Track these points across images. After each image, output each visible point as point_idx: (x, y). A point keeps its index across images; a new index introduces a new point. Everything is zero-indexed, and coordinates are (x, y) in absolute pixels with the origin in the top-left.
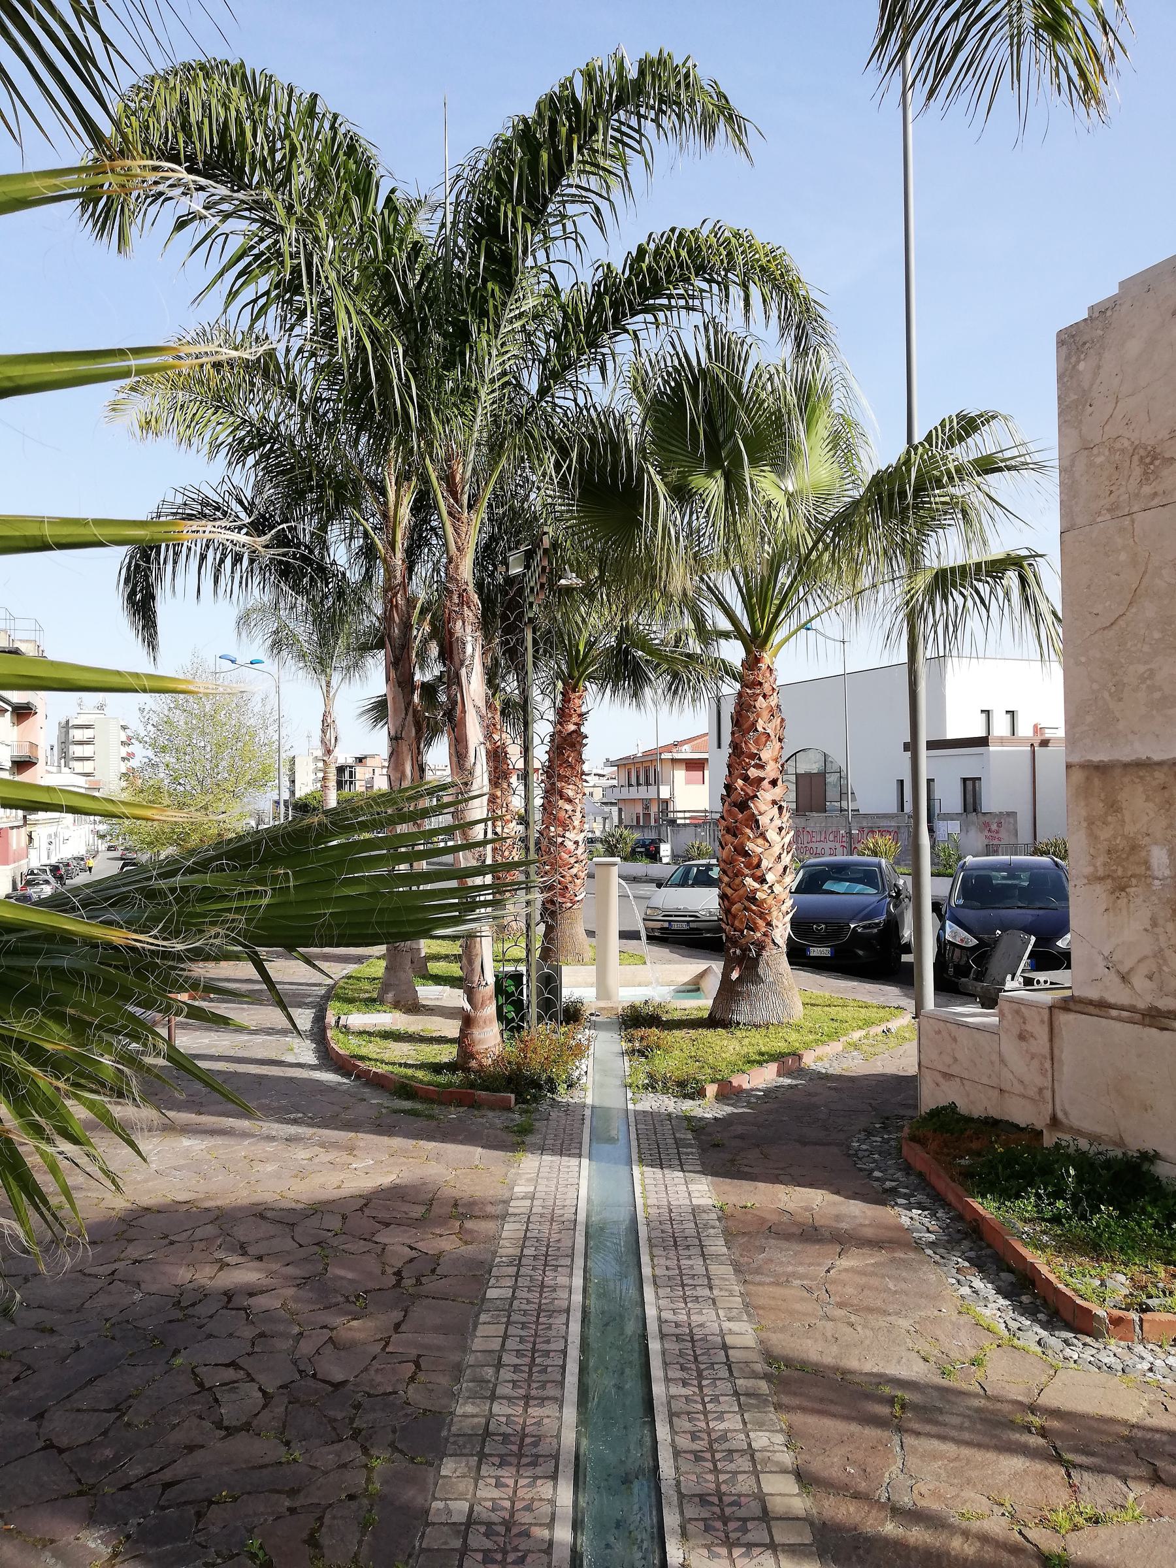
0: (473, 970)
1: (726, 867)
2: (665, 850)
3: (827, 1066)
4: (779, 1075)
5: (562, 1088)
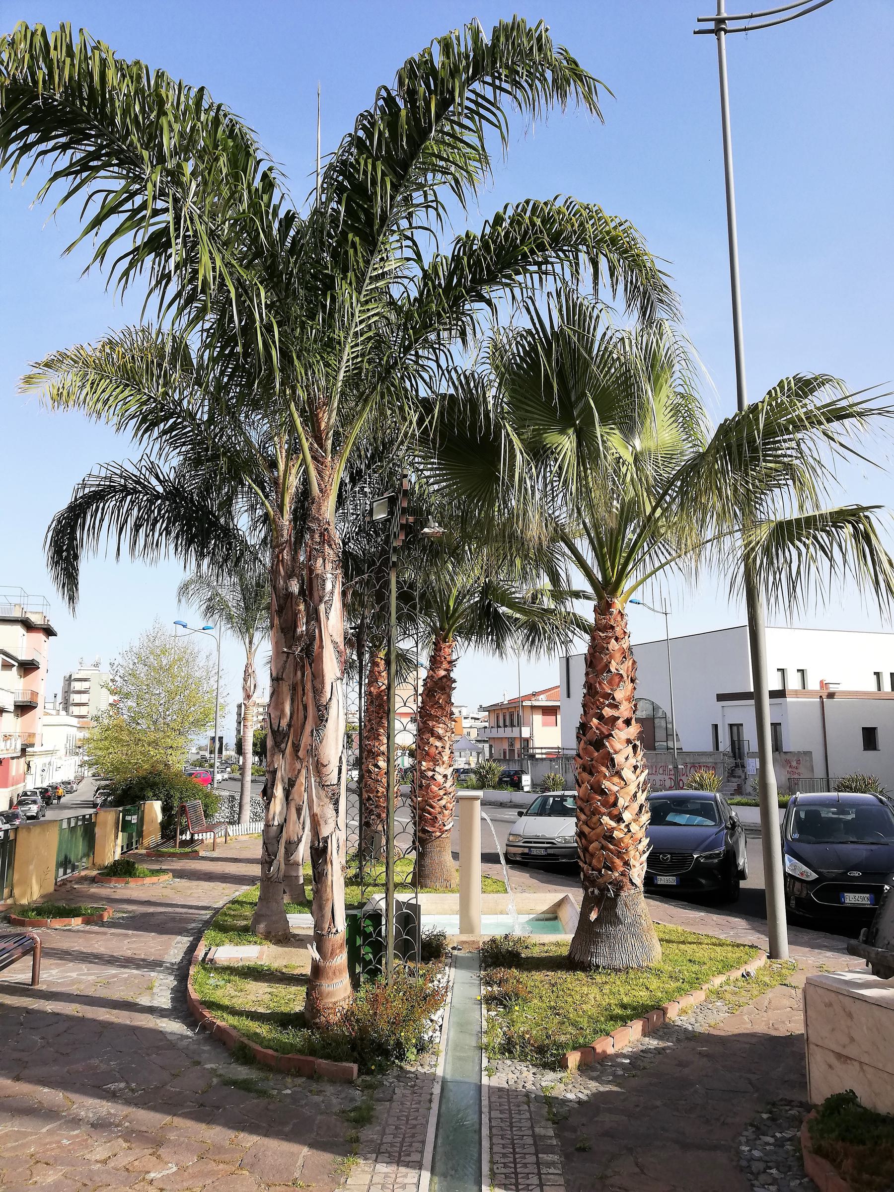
0: (323, 916)
1: (583, 805)
2: (526, 780)
3: (693, 1020)
4: (645, 1034)
5: (411, 1055)
